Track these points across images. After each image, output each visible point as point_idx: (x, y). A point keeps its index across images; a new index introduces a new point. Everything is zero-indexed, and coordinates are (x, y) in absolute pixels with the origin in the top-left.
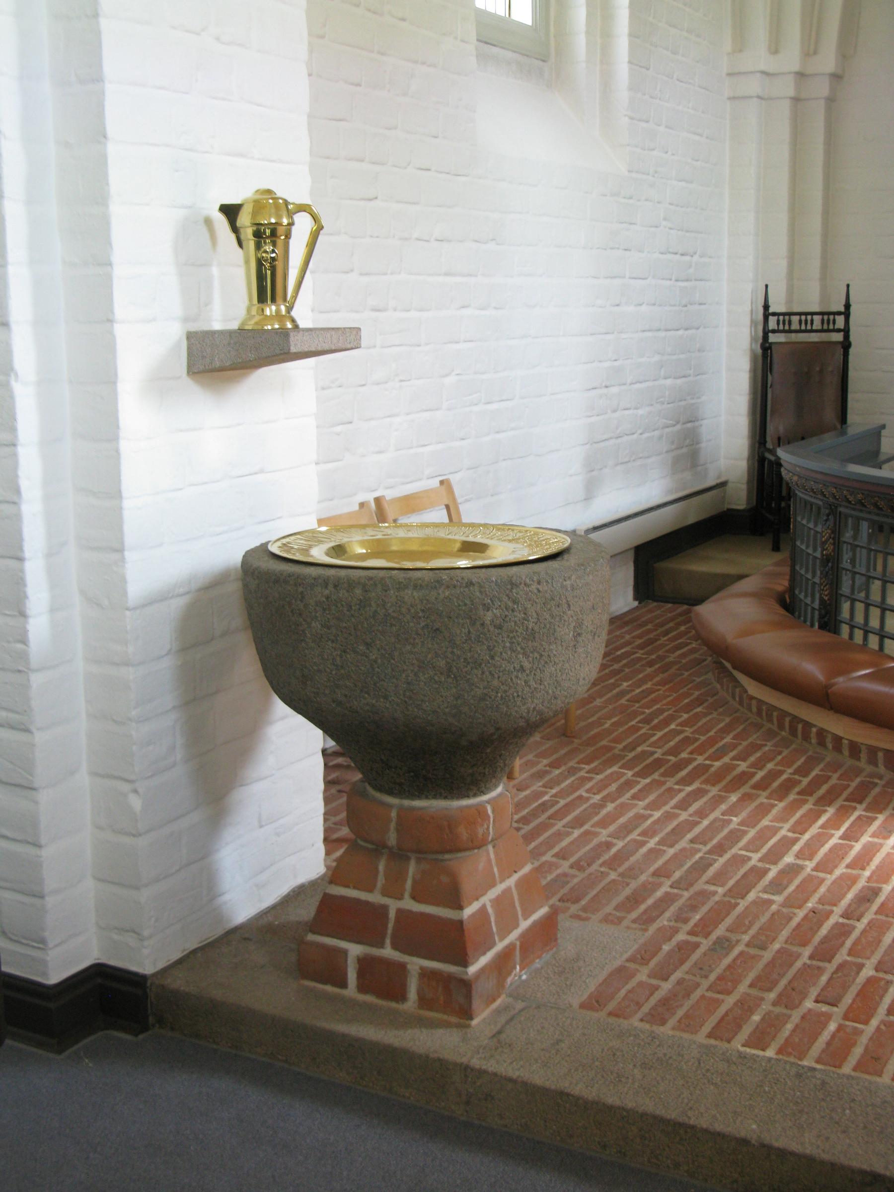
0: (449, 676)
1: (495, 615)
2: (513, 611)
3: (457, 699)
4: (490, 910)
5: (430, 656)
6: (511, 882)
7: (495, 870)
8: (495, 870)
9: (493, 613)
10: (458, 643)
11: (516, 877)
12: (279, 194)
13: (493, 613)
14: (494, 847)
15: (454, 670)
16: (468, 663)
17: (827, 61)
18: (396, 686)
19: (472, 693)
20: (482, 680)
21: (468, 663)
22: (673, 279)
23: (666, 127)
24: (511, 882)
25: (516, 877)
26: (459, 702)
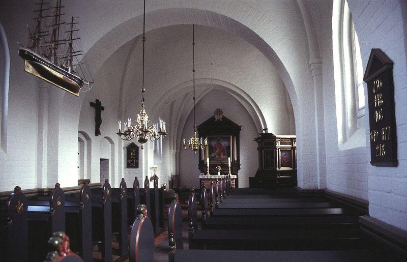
17: (179, 151)
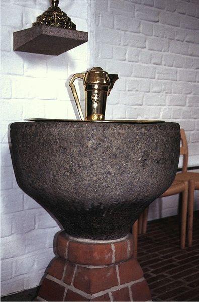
0: (71, 173)
1: (93, 143)
2: (103, 142)
3: (76, 185)
4: (130, 289)
5: (62, 162)
6: (129, 285)
7: (118, 278)
8: (118, 278)
9: (93, 142)
10: (75, 156)
11: (133, 283)
12: (104, 70)
13: (93, 142)
14: (119, 266)
15: (74, 170)
16: (80, 167)
18: (49, 177)
19: (83, 183)
20: (87, 176)
21: (80, 167)
22: (178, 79)
23: (157, 7)
24: (129, 285)
25: (133, 283)
26: (77, 187)
